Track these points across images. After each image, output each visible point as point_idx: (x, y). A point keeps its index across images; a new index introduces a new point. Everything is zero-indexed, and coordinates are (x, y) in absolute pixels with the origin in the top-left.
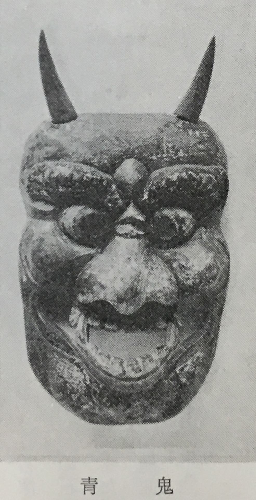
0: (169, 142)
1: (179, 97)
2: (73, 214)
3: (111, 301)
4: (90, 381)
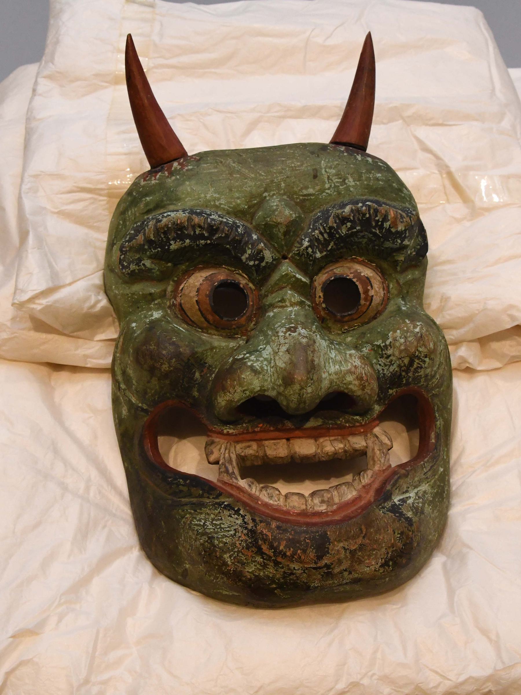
0: (330, 168)
1: (45, 336)
2: (197, 282)
3: (362, 195)
4: (254, 520)
